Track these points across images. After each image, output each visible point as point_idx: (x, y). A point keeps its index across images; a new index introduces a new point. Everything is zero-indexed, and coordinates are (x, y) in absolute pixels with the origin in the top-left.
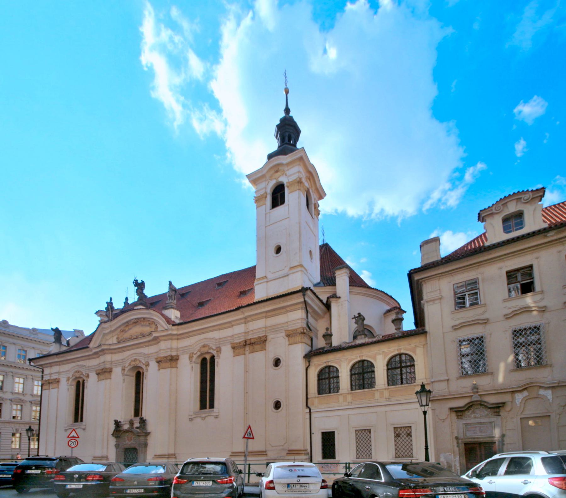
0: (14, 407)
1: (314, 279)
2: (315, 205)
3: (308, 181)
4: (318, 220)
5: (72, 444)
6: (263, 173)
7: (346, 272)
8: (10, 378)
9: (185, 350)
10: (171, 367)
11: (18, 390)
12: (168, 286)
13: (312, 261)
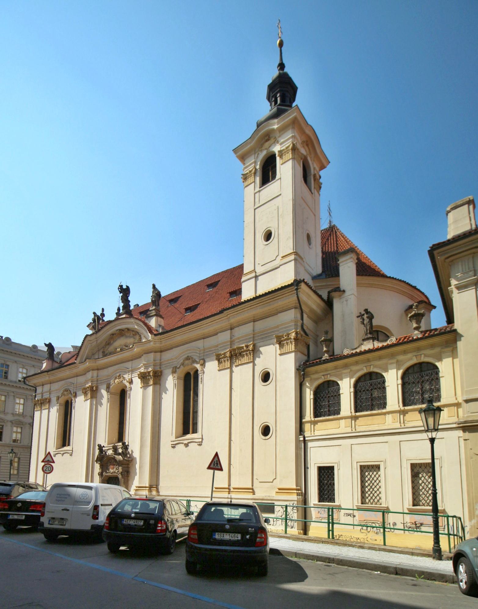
0: (15, 429)
1: (313, 270)
2: (315, 175)
3: (306, 147)
4: (320, 195)
5: (47, 470)
7: (352, 257)
8: (12, 398)
9: (168, 363)
11: (19, 412)
12: (152, 290)
13: (311, 246)
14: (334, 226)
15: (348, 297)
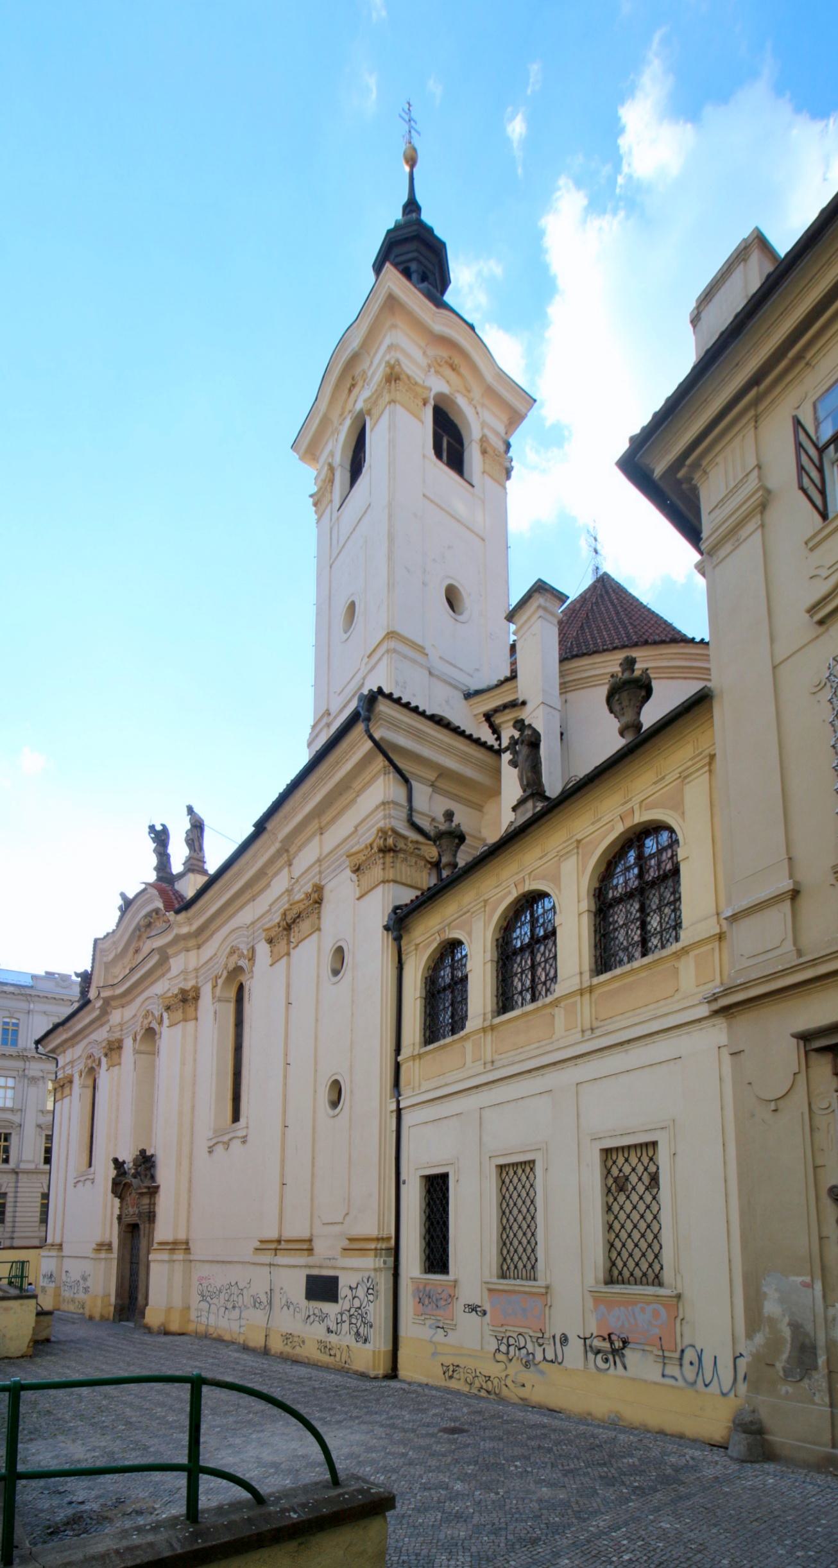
6: (321, 414)
10: (185, 1020)
14: (605, 574)
15: (532, 716)
